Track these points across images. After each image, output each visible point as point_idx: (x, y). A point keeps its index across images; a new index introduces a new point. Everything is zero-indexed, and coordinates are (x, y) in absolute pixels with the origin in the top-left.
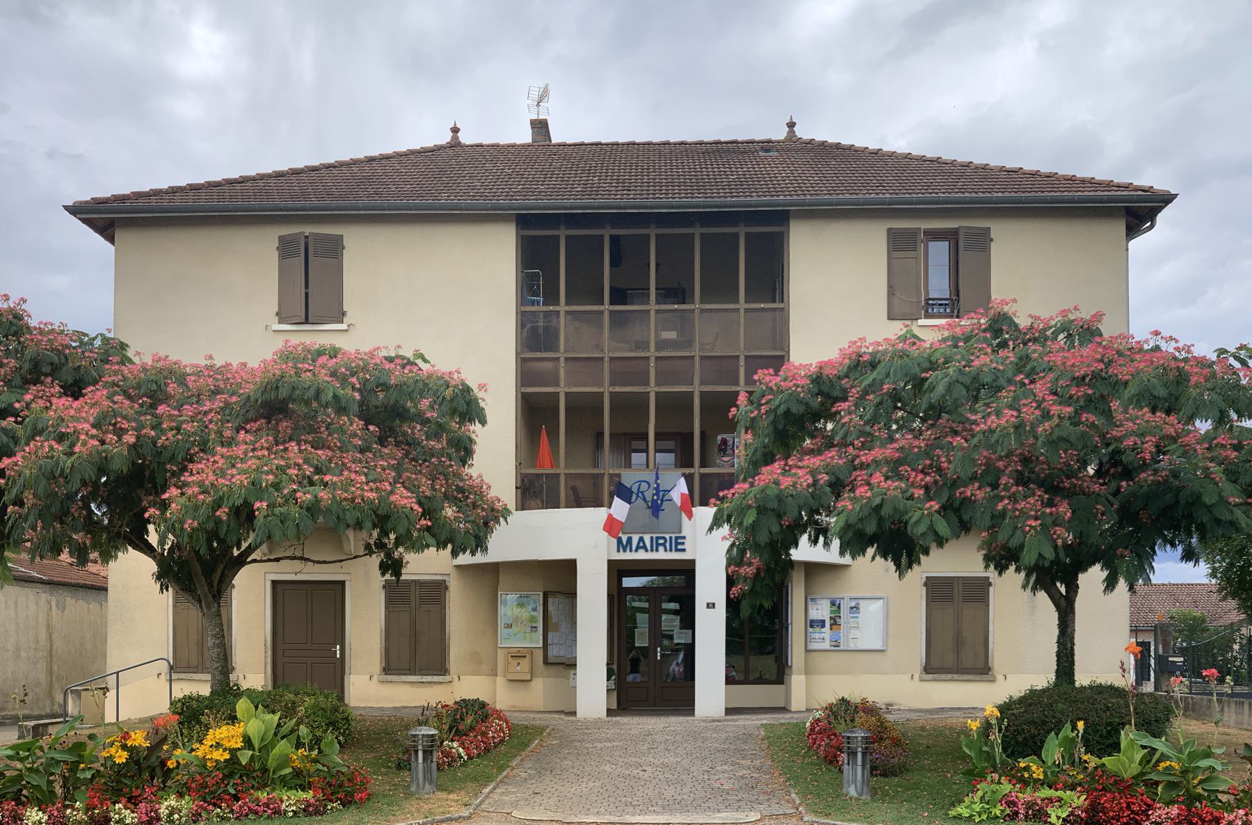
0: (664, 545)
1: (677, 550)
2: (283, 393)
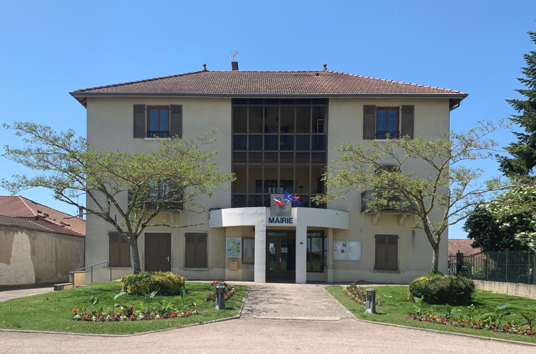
0: (285, 221)
1: (290, 223)
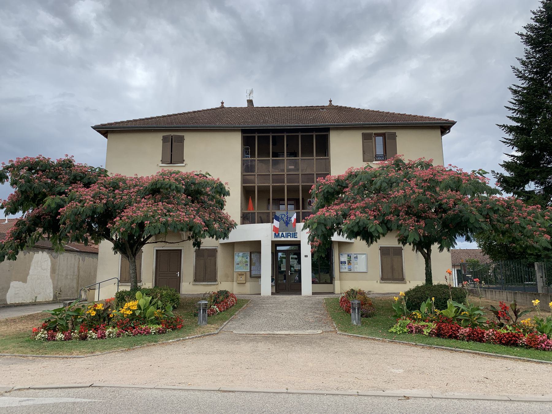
0: (290, 235)
1: (294, 237)
2: (158, 186)
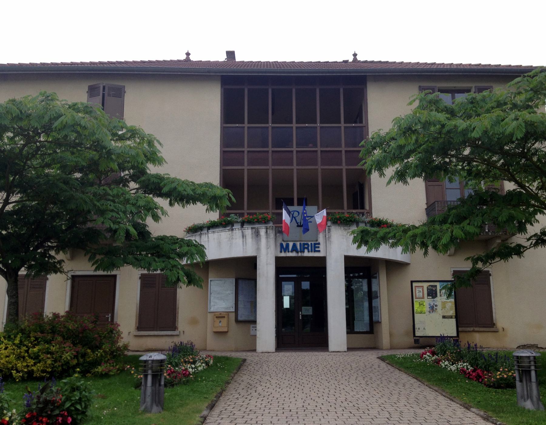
0: (308, 248)
1: (315, 251)
